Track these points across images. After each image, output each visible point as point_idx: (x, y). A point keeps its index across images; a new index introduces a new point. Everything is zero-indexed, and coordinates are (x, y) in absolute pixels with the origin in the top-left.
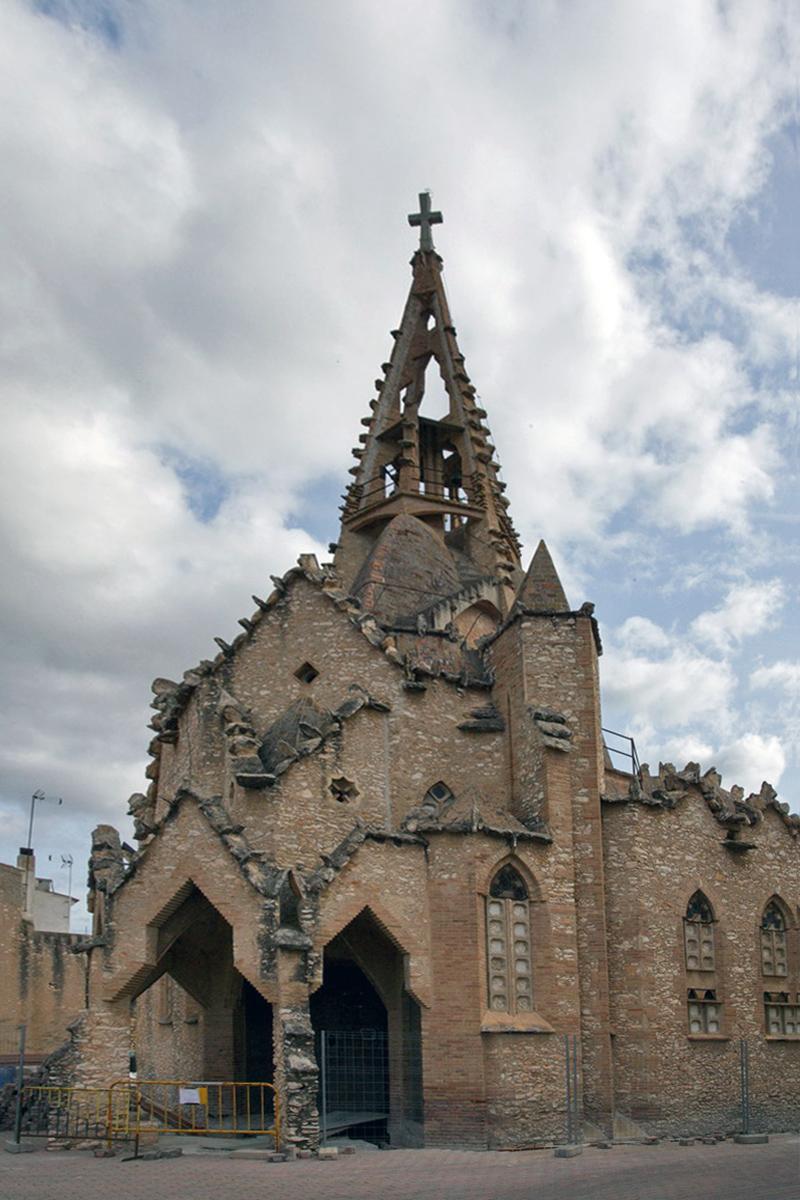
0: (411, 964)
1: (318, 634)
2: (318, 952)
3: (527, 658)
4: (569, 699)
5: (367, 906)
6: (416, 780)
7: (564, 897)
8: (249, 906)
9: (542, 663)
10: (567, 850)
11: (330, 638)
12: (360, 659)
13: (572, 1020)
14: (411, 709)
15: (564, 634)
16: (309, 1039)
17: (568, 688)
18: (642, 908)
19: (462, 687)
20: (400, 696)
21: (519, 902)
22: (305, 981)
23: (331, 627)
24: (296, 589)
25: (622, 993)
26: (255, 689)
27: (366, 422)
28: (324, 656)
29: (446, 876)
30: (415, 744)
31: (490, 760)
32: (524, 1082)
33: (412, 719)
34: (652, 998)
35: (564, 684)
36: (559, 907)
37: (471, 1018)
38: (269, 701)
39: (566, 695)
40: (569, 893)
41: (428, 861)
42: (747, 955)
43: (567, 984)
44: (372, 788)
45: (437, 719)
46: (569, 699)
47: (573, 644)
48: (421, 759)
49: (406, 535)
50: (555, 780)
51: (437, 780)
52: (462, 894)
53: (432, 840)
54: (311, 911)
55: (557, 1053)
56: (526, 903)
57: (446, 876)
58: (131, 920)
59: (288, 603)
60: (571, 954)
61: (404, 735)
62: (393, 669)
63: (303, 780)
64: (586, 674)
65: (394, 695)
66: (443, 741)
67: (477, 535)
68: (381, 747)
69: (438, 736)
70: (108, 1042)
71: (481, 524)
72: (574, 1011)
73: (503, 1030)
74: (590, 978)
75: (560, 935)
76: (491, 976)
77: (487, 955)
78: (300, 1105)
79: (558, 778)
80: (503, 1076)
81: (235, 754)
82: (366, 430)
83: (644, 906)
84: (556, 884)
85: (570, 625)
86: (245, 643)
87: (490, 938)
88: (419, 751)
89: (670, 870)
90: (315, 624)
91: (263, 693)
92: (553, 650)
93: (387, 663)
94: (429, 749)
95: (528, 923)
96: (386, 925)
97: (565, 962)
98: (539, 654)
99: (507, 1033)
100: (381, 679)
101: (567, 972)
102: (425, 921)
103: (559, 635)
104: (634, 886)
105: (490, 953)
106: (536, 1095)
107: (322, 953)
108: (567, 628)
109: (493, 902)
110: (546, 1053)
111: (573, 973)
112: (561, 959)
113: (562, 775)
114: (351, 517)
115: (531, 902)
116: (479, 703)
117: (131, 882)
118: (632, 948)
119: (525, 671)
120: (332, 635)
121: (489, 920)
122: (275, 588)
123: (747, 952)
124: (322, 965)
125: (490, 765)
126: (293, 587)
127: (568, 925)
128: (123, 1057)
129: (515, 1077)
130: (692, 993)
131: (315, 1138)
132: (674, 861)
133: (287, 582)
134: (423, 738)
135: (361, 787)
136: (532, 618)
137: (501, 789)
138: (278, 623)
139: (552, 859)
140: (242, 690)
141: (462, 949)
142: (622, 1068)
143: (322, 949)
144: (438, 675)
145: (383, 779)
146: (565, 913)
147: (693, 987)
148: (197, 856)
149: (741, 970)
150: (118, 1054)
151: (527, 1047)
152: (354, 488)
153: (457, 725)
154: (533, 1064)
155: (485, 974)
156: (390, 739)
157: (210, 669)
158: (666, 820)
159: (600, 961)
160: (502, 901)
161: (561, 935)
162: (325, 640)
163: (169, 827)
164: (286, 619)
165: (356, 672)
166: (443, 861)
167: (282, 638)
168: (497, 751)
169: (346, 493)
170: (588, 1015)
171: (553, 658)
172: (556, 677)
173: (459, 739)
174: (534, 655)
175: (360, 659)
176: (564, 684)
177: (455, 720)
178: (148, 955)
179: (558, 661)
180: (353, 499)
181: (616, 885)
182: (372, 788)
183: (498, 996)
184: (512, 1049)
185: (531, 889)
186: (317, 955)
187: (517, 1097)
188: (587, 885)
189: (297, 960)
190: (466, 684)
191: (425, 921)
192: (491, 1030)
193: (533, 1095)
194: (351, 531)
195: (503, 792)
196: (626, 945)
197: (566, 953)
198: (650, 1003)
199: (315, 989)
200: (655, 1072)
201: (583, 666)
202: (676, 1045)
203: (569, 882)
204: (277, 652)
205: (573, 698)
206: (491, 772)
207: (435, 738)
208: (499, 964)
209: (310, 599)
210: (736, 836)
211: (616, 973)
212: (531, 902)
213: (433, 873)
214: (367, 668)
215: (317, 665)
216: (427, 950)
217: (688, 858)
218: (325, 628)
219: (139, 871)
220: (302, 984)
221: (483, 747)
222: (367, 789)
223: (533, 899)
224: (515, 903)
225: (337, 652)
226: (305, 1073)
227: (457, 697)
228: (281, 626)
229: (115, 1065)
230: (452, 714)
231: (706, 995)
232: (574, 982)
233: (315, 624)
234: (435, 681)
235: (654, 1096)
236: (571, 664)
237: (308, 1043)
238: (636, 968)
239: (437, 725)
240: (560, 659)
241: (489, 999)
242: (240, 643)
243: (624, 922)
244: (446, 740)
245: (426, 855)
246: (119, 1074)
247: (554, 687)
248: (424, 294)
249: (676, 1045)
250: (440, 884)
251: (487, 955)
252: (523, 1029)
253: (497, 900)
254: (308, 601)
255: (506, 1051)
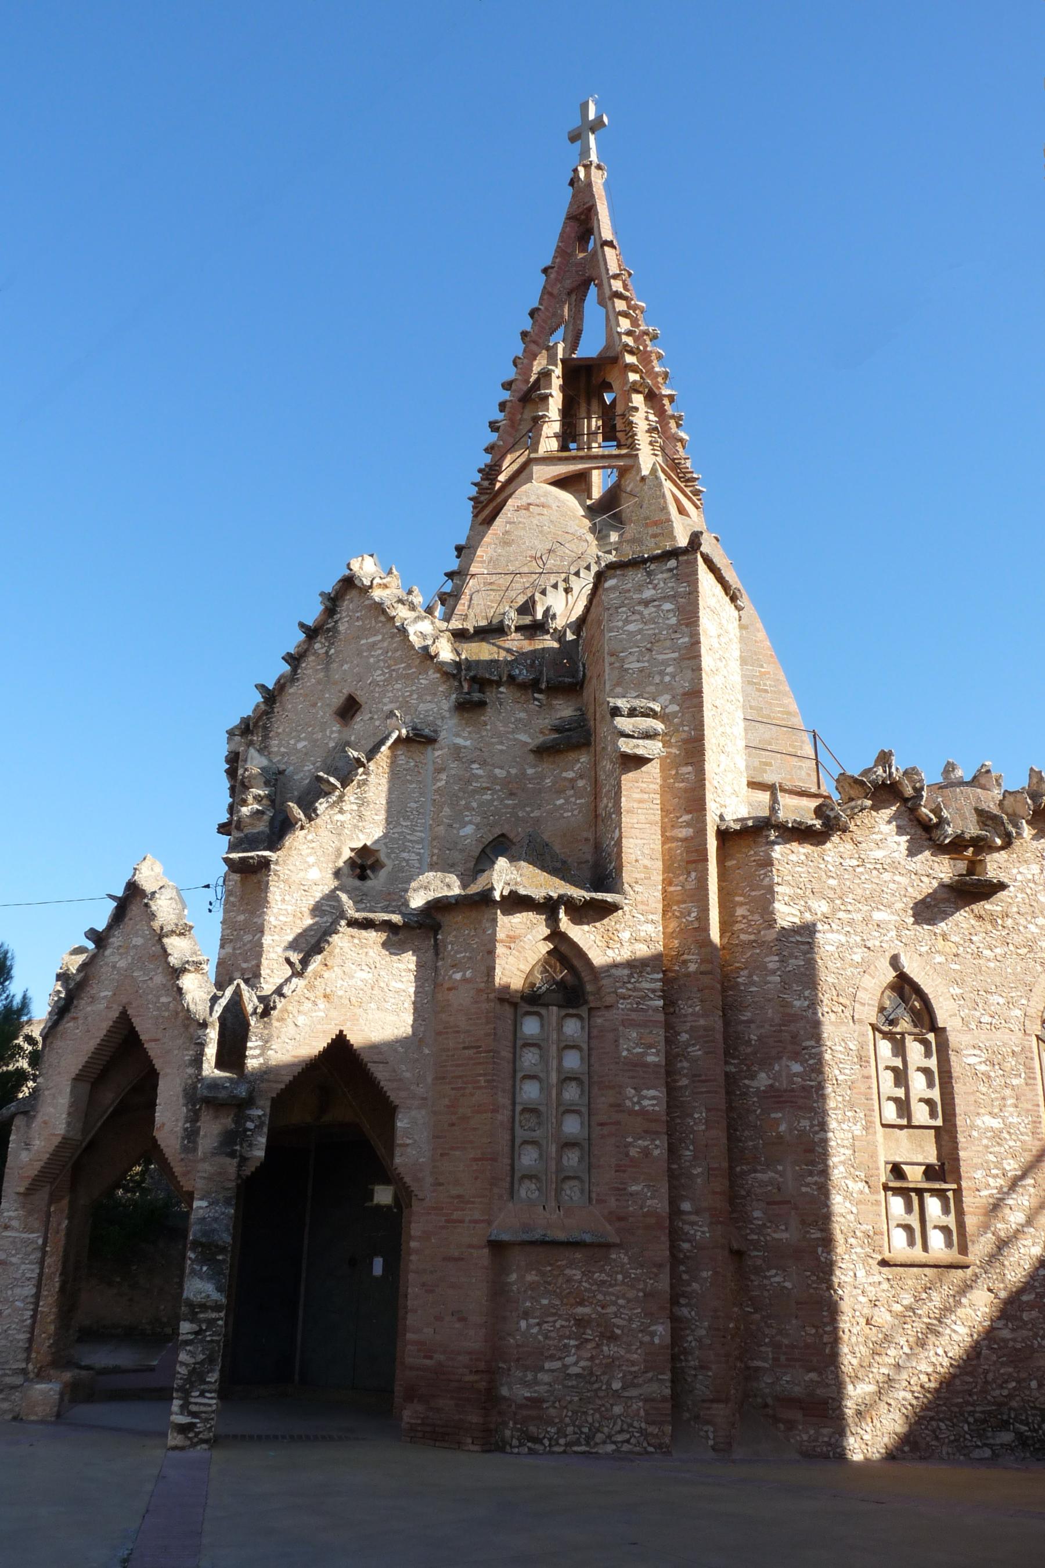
0: (399, 1124)
1: (365, 654)
2: (262, 1108)
3: (611, 631)
4: (667, 679)
5: (341, 1032)
6: (466, 837)
7: (645, 997)
8: (180, 1042)
9: (630, 633)
10: (650, 917)
11: (379, 655)
12: (407, 677)
13: (653, 1221)
14: (466, 734)
15: (662, 585)
16: (222, 1250)
17: (665, 663)
18: (789, 1010)
19: (540, 691)
20: (450, 718)
21: (571, 1011)
22: (232, 1154)
23: (380, 641)
24: (346, 603)
25: (755, 1171)
26: (292, 742)
27: (507, 386)
28: (369, 682)
29: (458, 976)
30: (469, 782)
31: (572, 792)
32: (562, 1337)
33: (465, 747)
34: (809, 1179)
35: (660, 657)
36: (634, 1015)
37: (477, 1216)
38: (306, 754)
39: (662, 673)
40: (653, 991)
41: (437, 954)
42: (1008, 1092)
43: (646, 1152)
44: (405, 855)
45: (502, 743)
46: (667, 679)
47: (674, 596)
48: (474, 805)
49: (527, 509)
50: (636, 805)
51: (497, 831)
52: (476, 1002)
53: (446, 920)
54: (260, 1043)
55: (623, 1283)
56: (583, 1012)
57: (458, 976)
58: (59, 1073)
59: (336, 622)
60: (653, 1098)
61: (453, 772)
62: (444, 682)
63: (311, 854)
64: (691, 637)
65: (443, 718)
66: (508, 772)
67: (628, 489)
68: (422, 794)
69: (502, 768)
70: (13, 1256)
71: (634, 472)
72: (659, 1204)
73: (526, 1237)
74: (693, 1143)
75: (636, 1065)
76: (518, 1141)
77: (514, 1104)
78: (192, 1361)
79: (640, 801)
80: (523, 1324)
81: (242, 831)
82: (506, 395)
83: (792, 1006)
84: (631, 976)
85: (671, 570)
86: (288, 684)
87: (519, 1075)
88: (475, 791)
89: (843, 939)
90: (363, 642)
91: (300, 745)
92: (646, 612)
93: (438, 675)
94: (488, 789)
95: (585, 1046)
96: (366, 1060)
97: (643, 1113)
98: (627, 622)
99: (532, 1243)
100: (429, 698)
101: (646, 1132)
102: (427, 1051)
103: (654, 588)
104: (773, 972)
105: (518, 1100)
106: (582, 1364)
107: (268, 1110)
108: (665, 575)
109: (528, 1013)
110: (603, 1282)
111: (657, 1133)
112: (637, 1108)
113: (646, 796)
114: (480, 506)
115: (590, 1009)
116: (564, 710)
117: (65, 1020)
118: (771, 1086)
119: (606, 651)
120: (380, 652)
121: (519, 1043)
122: (322, 607)
123: (1006, 1085)
124: (265, 1130)
125: (573, 799)
126: (344, 600)
127: (650, 1047)
128: (29, 1279)
129: (545, 1326)
130: (897, 1171)
131: (207, 1420)
132: (851, 923)
133: (337, 593)
134: (480, 772)
135: (388, 856)
136: (618, 572)
137: (585, 834)
138: (323, 651)
139: (626, 935)
140: (279, 746)
141: (472, 1095)
142: (757, 1316)
143: (268, 1103)
144: (505, 679)
145: (421, 841)
146: (644, 1024)
147: (898, 1159)
148: (135, 974)
149: (996, 1123)
150: (23, 1274)
151: (568, 1272)
152: (487, 470)
153: (530, 747)
154: (581, 1303)
155: (507, 1137)
156: (436, 780)
157: (248, 726)
158: (835, 847)
159: (708, 1110)
160: (543, 1011)
161: (636, 1065)
162: (372, 660)
163: (114, 936)
164: (333, 644)
165: (403, 695)
166: (457, 952)
167: (327, 669)
168: (581, 777)
169: (478, 477)
170: (689, 1213)
171: (645, 623)
172: (650, 650)
173: (535, 766)
174: (620, 624)
175: (407, 677)
176: (660, 657)
177: (530, 741)
178: (69, 1124)
179: (653, 626)
180: (486, 483)
181: (745, 973)
182: (405, 855)
183: (530, 1177)
184: (543, 1274)
185: (589, 988)
186: (260, 1113)
187: (547, 1365)
188: (688, 975)
189: (227, 1122)
190: (543, 686)
191: (427, 1051)
192: (505, 1237)
193: (576, 1364)
194: (480, 524)
195: (587, 840)
196: (763, 1080)
197: (645, 1097)
198: (804, 1189)
199: (249, 1169)
200: (816, 1327)
201: (687, 625)
202: (861, 1273)
203: (653, 972)
204: (320, 687)
205: (673, 676)
206: (572, 811)
207: (497, 771)
208: (533, 1120)
209: (361, 611)
210: (979, 869)
211: (746, 1133)
212: (590, 1009)
213: (442, 972)
214: (414, 688)
215: (361, 697)
216: (425, 1099)
217: (877, 916)
218: (374, 644)
219: (75, 1002)
220: (228, 1160)
221: (564, 774)
222: (397, 858)
223: (592, 1005)
224: (563, 1012)
225: (383, 674)
226: (204, 1307)
227: (533, 706)
228: (327, 652)
229: (17, 1291)
230: (525, 732)
231: (925, 1173)
232: (659, 1149)
233: (363, 642)
234: (502, 689)
235: (813, 1376)
236: (670, 626)
237: (220, 1257)
238: (777, 1122)
239: (501, 751)
240: (655, 623)
241: (512, 1183)
242: (282, 685)
243: (760, 1039)
244: (513, 771)
245: (436, 945)
246: (22, 1305)
247: (646, 664)
248: (581, 214)
249: (861, 1273)
250: (449, 989)
251: (514, 1104)
252: (561, 1236)
253: (535, 1009)
254: (358, 614)
255: (531, 1277)
